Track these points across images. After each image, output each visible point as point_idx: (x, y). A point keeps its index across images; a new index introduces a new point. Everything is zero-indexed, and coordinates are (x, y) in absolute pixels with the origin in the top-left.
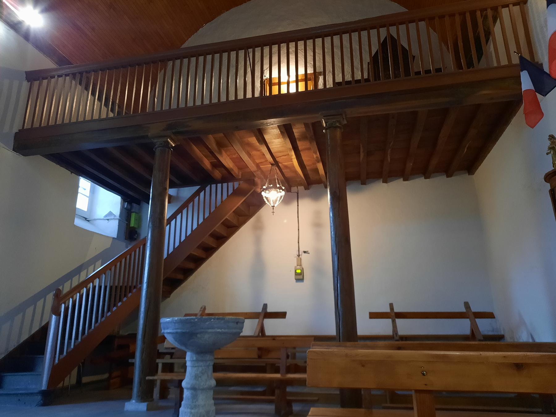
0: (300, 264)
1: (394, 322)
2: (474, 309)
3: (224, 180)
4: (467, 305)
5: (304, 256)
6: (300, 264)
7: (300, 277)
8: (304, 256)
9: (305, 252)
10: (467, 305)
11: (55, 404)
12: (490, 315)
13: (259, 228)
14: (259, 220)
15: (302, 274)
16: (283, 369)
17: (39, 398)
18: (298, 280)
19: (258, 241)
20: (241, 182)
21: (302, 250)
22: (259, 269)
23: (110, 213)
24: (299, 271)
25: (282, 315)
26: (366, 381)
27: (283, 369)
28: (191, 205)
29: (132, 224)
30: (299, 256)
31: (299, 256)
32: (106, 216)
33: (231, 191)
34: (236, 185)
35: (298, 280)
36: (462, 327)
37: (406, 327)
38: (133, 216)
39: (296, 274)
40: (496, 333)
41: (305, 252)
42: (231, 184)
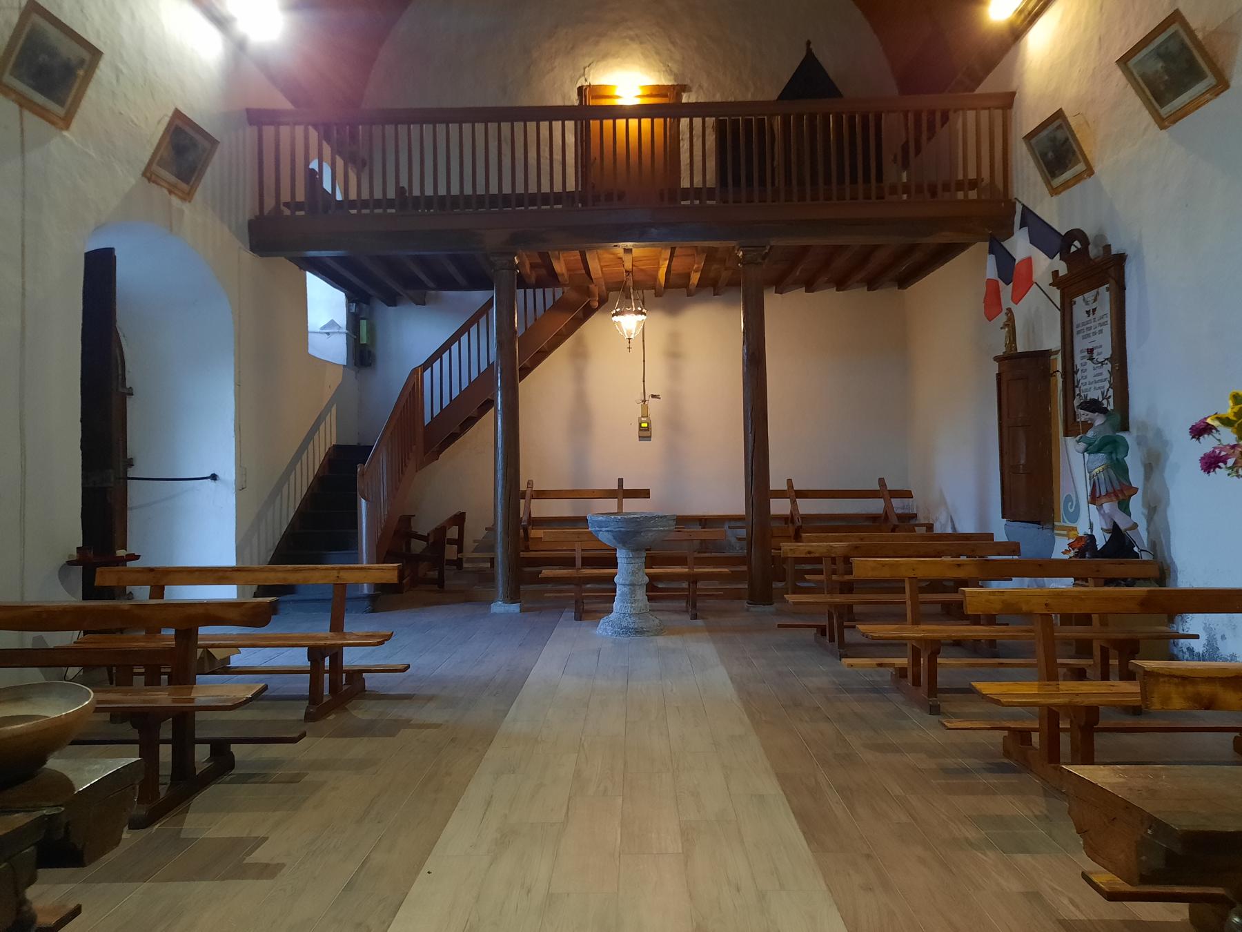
0: (645, 414)
1: (794, 503)
2: (891, 486)
3: (540, 284)
4: (882, 481)
5: (652, 403)
6: (645, 414)
7: (645, 434)
8: (652, 403)
9: (653, 396)
10: (882, 481)
11: (389, 610)
12: (907, 494)
13: (580, 355)
14: (580, 342)
15: (648, 429)
16: (579, 563)
17: (366, 603)
18: (642, 438)
19: (579, 376)
20: (566, 289)
21: (648, 393)
22: (581, 419)
23: (332, 323)
24: (644, 425)
25: (644, 494)
26: (118, 636)
27: (579, 563)
28: (483, 320)
29: (364, 340)
30: (644, 401)
31: (644, 401)
32: (324, 327)
33: (550, 303)
34: (559, 293)
35: (642, 438)
36: (875, 506)
37: (807, 507)
38: (363, 323)
39: (641, 429)
40: (907, 511)
41: (653, 396)
42: (549, 291)
